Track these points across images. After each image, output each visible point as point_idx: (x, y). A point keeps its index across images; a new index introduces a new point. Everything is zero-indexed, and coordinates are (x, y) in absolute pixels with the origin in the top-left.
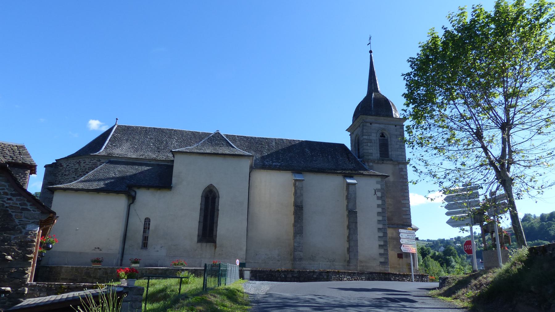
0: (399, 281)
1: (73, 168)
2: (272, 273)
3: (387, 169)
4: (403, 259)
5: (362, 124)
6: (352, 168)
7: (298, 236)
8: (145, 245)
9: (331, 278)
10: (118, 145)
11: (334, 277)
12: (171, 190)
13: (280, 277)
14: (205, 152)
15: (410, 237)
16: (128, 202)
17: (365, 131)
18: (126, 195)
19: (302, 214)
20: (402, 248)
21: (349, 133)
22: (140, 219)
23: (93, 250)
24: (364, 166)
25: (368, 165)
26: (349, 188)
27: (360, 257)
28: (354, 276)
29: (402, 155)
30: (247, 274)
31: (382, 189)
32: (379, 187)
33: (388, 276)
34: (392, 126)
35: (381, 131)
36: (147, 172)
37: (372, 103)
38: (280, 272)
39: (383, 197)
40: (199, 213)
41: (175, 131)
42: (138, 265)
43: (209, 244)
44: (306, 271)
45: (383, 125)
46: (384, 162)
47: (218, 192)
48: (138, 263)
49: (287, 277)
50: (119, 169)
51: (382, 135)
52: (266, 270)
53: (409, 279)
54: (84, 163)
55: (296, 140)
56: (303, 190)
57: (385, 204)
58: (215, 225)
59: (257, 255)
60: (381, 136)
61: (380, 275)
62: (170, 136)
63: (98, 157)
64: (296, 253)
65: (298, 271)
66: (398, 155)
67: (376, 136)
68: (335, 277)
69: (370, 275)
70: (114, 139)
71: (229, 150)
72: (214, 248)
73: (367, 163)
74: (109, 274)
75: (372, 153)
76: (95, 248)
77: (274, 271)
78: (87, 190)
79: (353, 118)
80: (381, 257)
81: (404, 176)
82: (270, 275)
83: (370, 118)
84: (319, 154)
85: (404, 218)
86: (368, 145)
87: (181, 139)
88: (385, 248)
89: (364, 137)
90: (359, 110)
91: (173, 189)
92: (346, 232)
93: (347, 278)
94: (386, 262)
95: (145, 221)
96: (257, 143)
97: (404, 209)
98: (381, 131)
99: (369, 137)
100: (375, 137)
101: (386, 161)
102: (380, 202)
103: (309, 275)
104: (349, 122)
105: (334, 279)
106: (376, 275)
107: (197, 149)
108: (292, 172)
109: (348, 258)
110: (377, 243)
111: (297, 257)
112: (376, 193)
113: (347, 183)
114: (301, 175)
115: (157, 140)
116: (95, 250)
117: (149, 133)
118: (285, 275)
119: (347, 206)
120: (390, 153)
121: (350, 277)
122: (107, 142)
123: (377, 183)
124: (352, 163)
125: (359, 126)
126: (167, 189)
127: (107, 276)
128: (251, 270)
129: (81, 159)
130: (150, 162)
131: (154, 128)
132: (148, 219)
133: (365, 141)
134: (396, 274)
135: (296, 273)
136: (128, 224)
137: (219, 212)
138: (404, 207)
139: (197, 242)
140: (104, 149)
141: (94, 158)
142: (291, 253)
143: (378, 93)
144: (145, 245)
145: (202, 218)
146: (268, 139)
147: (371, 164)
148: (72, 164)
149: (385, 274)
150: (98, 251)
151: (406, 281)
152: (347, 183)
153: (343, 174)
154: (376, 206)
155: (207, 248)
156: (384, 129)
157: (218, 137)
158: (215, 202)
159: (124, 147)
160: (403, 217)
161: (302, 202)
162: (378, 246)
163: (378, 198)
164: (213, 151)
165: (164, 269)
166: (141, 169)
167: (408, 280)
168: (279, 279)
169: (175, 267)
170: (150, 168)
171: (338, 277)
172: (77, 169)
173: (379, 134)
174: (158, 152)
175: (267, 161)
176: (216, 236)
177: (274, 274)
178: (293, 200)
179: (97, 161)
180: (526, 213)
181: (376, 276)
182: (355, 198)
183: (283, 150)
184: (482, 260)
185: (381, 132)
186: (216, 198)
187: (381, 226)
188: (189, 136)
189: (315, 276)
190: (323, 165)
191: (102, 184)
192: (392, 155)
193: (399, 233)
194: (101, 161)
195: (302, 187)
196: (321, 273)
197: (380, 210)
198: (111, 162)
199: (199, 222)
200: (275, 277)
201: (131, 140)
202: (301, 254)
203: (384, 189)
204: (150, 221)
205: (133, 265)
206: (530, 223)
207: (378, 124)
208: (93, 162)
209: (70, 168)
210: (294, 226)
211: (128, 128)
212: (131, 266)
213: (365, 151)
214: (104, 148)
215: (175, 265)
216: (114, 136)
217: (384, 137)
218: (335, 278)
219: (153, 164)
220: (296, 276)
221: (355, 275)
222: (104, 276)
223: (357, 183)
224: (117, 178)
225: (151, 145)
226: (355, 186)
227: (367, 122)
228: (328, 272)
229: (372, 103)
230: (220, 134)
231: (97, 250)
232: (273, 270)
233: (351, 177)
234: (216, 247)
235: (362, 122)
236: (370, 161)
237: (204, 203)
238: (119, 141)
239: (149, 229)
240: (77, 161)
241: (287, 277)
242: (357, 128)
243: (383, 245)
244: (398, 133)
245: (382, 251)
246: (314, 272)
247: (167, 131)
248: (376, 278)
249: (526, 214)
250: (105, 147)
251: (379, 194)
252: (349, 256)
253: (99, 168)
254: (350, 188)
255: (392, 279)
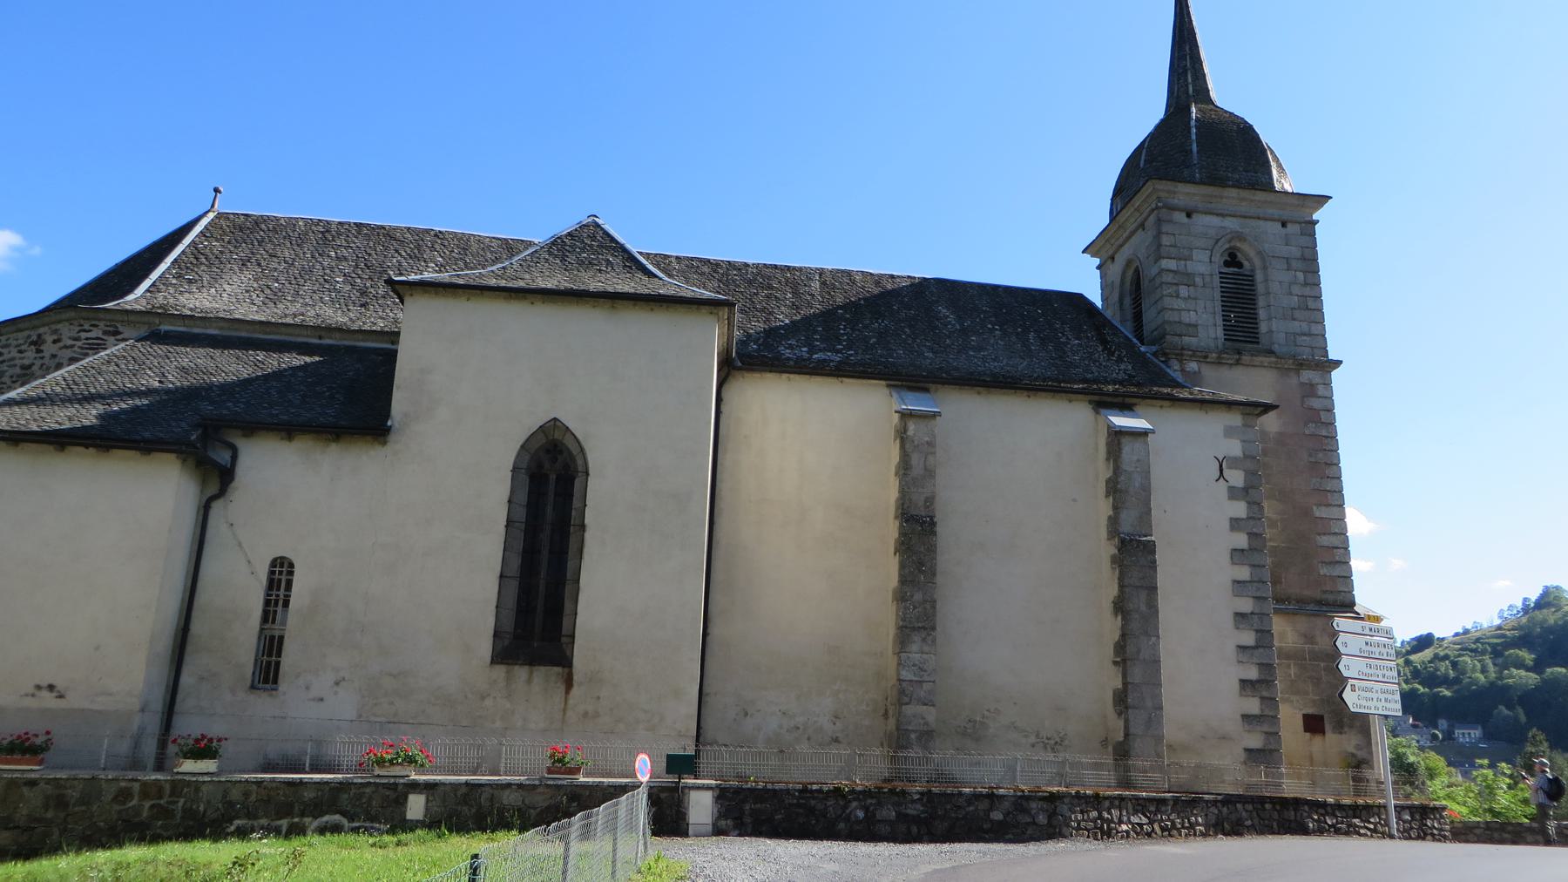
0: (1338, 832)
1: (15, 365)
2: (813, 802)
3: (1254, 382)
4: (1327, 735)
5: (1152, 218)
6: (1121, 376)
7: (917, 638)
8: (267, 673)
9: (1068, 826)
10: (206, 278)
11: (1080, 817)
12: (384, 443)
13: (848, 819)
14: (533, 286)
15: (1376, 650)
16: (202, 492)
17: (1165, 240)
18: (184, 461)
19: (932, 549)
20: (1349, 697)
21: (1097, 261)
22: (249, 562)
23: (27, 695)
24: (1168, 370)
25: (1183, 370)
26: (1120, 450)
27: (1170, 732)
28: (1162, 813)
29: (1309, 335)
30: (701, 807)
31: (1246, 457)
32: (1235, 448)
33: (1295, 810)
34: (1270, 223)
35: (1230, 242)
36: (300, 374)
37: (1194, 137)
38: (844, 797)
39: (1253, 487)
40: (503, 540)
41: (437, 235)
42: (209, 765)
43: (541, 672)
44: (960, 794)
45: (1234, 220)
46: (1244, 357)
47: (582, 450)
48: (215, 758)
49: (878, 817)
50: (185, 362)
51: (1232, 260)
52: (782, 786)
53: (1375, 824)
54: (55, 342)
55: (898, 277)
56: (934, 453)
57: (1260, 519)
58: (568, 589)
59: (746, 714)
60: (1227, 264)
61: (1265, 810)
62: (416, 251)
63: (109, 317)
64: (909, 710)
65: (922, 794)
66: (1295, 334)
67: (1211, 262)
68: (1083, 820)
69: (1225, 809)
70: (192, 260)
71: (633, 284)
72: (563, 688)
73: (1176, 362)
74: (74, 805)
75: (1195, 326)
76: (39, 687)
77: (820, 791)
78: (7, 435)
79: (1112, 205)
80: (1249, 731)
81: (1322, 413)
82: (801, 811)
83: (1185, 194)
84: (989, 326)
85: (1325, 576)
86: (1181, 295)
87: (456, 264)
88: (1265, 694)
89: (1165, 263)
90: (1142, 165)
91: (392, 437)
92: (1111, 628)
93: (1133, 824)
94: (1271, 751)
95: (272, 573)
96: (750, 282)
97: (1325, 540)
98: (1230, 242)
99: (1183, 262)
100: (1204, 264)
101: (1252, 355)
102: (1240, 509)
103: (971, 808)
104: (1098, 218)
105: (1078, 828)
106: (1250, 807)
107: (497, 277)
108: (888, 386)
109: (1122, 734)
110: (1233, 672)
111: (910, 728)
112: (1226, 472)
113: (1109, 427)
114: (928, 395)
115: (362, 265)
116: (33, 695)
117: (333, 240)
118: (866, 809)
119: (1113, 522)
120: (1263, 327)
121: (1146, 816)
122: (163, 267)
123: (1229, 432)
124: (1122, 361)
125: (1142, 226)
126: (369, 438)
127: (62, 815)
128: (718, 786)
129: (47, 328)
130: (320, 338)
131: (358, 225)
132: (286, 565)
133: (1168, 278)
134: (1324, 805)
135: (913, 801)
136: (200, 584)
137: (588, 535)
138: (1324, 534)
139: (492, 663)
140: (148, 291)
141: (94, 319)
142: (886, 710)
143: (1212, 106)
144: (267, 674)
145: (516, 562)
146: (794, 268)
147: (1193, 366)
148: (11, 348)
149: (1284, 803)
150: (48, 700)
151: (1362, 831)
152: (1109, 427)
153: (1092, 394)
154: (1227, 525)
155: (536, 684)
156: (1241, 237)
157: (593, 238)
158: (571, 495)
159: (226, 286)
160: (1322, 572)
161: (930, 501)
162: (1237, 686)
163: (1233, 493)
164: (565, 285)
165: (327, 783)
166: (275, 363)
167: (1372, 826)
168: (842, 825)
169: (377, 771)
170: (317, 359)
171: (1094, 821)
172: (30, 366)
173: (1222, 255)
174: (361, 306)
175: (791, 347)
176: (573, 636)
177: (820, 806)
178: (893, 494)
179: (105, 333)
180: (1548, 585)
181: (1247, 811)
182: (1146, 490)
183: (854, 308)
184: (1414, 720)
185: (1227, 246)
186: (574, 479)
187: (1246, 605)
188: (491, 252)
189: (997, 816)
190: (1007, 364)
191: (89, 416)
192: (1270, 332)
193: (1335, 634)
194: (120, 333)
195: (930, 444)
196: (1021, 802)
197: (1241, 540)
198: (156, 337)
199: (501, 576)
200: (825, 816)
201: (259, 265)
202: (930, 714)
203: (1255, 458)
204: (291, 573)
205: (189, 766)
206: (1559, 614)
207: (1217, 215)
208: (87, 339)
209: (5, 364)
210: (901, 597)
211: (258, 222)
212: (180, 770)
213: (1168, 316)
214: (147, 287)
215: (381, 762)
216: (196, 248)
217: (1240, 265)
218: (1083, 824)
219: (330, 346)
220: (914, 812)
221: (1163, 809)
222: (50, 814)
223: (1153, 431)
224: (168, 392)
225: (338, 282)
226: (1146, 443)
227: (1173, 208)
228: (1053, 798)
229: (1194, 137)
230: (602, 229)
231: (45, 694)
232: (815, 787)
233: (1125, 408)
234: (569, 683)
235: (1157, 208)
236: (1190, 353)
237: (523, 497)
238: (210, 265)
239: (286, 604)
240: (29, 337)
241: (878, 817)
242: (1133, 233)
243: (1258, 681)
244: (1294, 251)
245: (1253, 706)
246: (992, 797)
247: (408, 235)
248: (1249, 823)
249: (1547, 587)
250: (153, 285)
251: (1236, 478)
252: (1121, 723)
253: (101, 357)
254: (1124, 452)
255: (1311, 825)
